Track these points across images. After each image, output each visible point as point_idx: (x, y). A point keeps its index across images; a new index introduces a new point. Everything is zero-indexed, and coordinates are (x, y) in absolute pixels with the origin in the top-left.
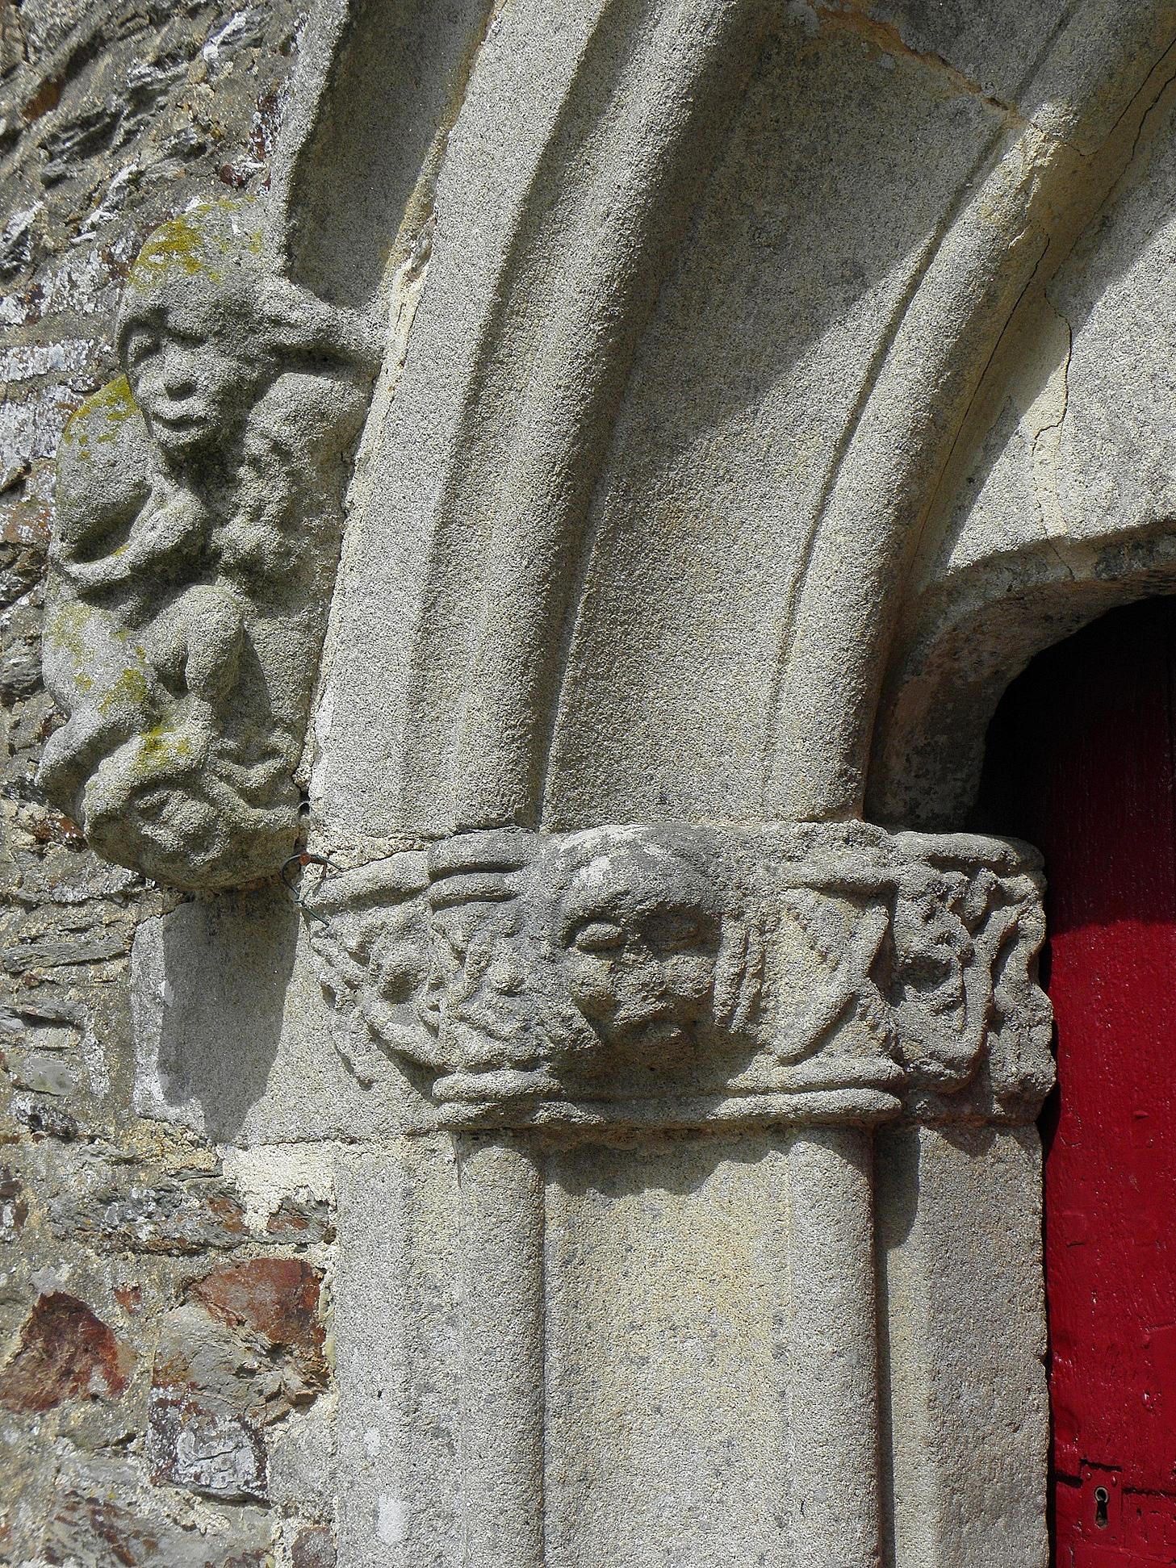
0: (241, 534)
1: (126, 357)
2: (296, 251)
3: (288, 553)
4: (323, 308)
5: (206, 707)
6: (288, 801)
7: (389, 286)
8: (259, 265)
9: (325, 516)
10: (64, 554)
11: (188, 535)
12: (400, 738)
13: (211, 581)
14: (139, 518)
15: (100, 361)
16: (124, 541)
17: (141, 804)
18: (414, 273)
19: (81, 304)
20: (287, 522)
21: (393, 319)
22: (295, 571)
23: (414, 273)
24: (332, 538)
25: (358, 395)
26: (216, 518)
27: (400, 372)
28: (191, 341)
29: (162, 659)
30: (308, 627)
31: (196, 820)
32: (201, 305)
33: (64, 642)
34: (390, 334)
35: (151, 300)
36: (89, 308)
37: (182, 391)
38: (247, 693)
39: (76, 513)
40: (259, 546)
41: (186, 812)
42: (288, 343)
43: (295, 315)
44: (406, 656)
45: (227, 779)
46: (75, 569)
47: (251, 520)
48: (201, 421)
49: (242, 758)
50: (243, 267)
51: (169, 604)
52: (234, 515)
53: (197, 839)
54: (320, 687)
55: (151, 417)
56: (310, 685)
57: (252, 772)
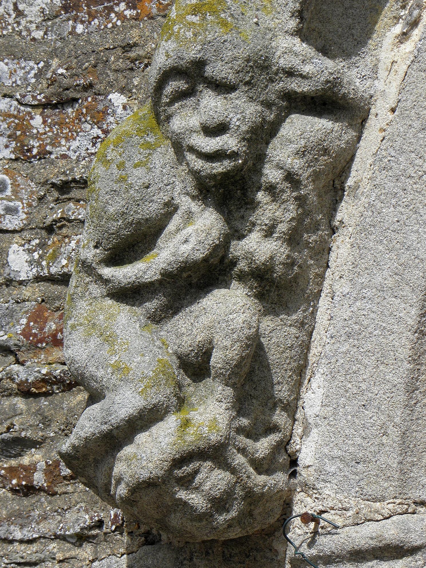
0: (257, 247)
1: (160, 98)
2: (306, 15)
3: (293, 264)
4: (329, 63)
5: (229, 391)
6: (282, 469)
7: (378, 46)
8: (272, 25)
9: (320, 233)
10: (97, 260)
11: (215, 248)
12: (397, 420)
13: (227, 286)
14: (166, 231)
15: (52, 82)
16: (151, 249)
17: (179, 473)
18: (404, 36)
19: (28, 30)
20: (293, 239)
21: (382, 73)
22: (296, 278)
23: (404, 36)
24: (323, 251)
25: (352, 133)
26: (236, 233)
27: (391, 116)
28: (222, 87)
29: (185, 349)
30: (303, 324)
31: (222, 486)
32: (235, 59)
33: (95, 333)
34: (379, 85)
35: (193, 53)
36: (38, 34)
37: (219, 129)
38: (256, 379)
39: (114, 226)
40: (272, 258)
41: (213, 479)
42: (299, 90)
43: (307, 69)
44: (405, 353)
45: (243, 451)
46: (107, 272)
47: (266, 236)
48: (234, 155)
49: (253, 434)
50: (262, 26)
51: (191, 303)
52: (250, 231)
53: (220, 503)
54: (308, 373)
55: (180, 148)
56: (301, 372)
57: (258, 445)
